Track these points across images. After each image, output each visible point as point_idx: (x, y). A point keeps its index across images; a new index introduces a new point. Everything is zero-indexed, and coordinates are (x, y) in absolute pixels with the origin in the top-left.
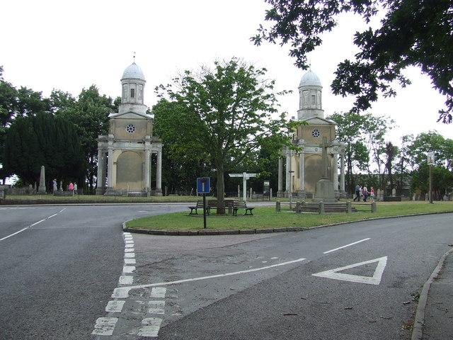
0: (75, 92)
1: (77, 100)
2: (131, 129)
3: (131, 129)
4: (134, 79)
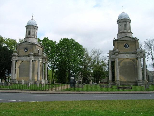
0: (80, 44)
1: (56, 44)
2: (127, 46)
3: (127, 46)
4: (34, 26)
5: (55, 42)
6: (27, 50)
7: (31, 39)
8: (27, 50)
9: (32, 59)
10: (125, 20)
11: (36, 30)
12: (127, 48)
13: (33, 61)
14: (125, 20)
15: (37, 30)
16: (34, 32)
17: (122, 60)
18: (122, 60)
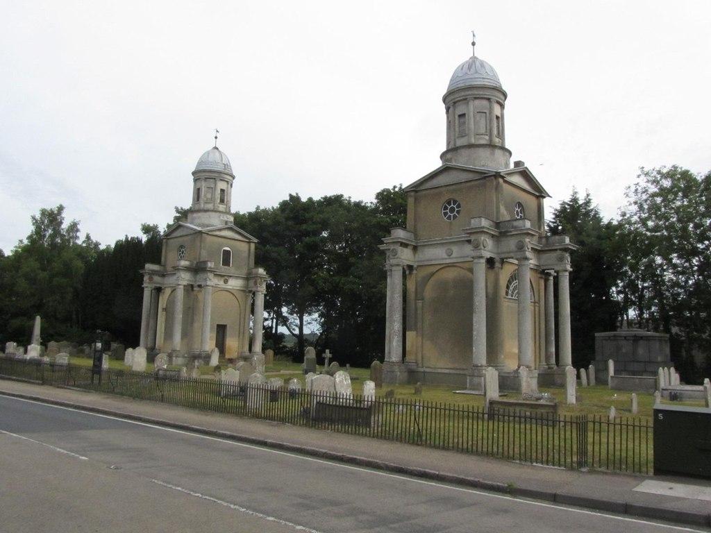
5: (141, 241)
6: (458, 212)
7: (200, 214)
8: (458, 212)
9: (488, 255)
10: (463, 94)
11: (497, 110)
12: (450, 217)
13: (490, 262)
14: (463, 94)
15: (502, 106)
16: (488, 114)
17: (433, 274)
18: (433, 274)
